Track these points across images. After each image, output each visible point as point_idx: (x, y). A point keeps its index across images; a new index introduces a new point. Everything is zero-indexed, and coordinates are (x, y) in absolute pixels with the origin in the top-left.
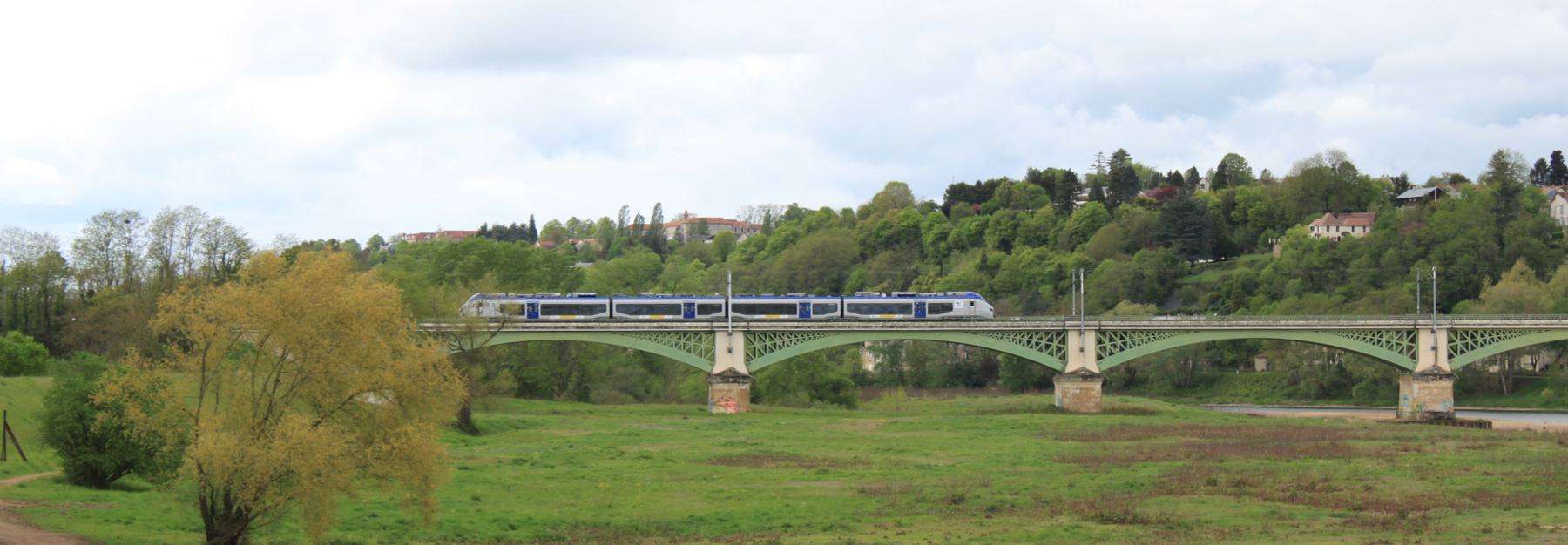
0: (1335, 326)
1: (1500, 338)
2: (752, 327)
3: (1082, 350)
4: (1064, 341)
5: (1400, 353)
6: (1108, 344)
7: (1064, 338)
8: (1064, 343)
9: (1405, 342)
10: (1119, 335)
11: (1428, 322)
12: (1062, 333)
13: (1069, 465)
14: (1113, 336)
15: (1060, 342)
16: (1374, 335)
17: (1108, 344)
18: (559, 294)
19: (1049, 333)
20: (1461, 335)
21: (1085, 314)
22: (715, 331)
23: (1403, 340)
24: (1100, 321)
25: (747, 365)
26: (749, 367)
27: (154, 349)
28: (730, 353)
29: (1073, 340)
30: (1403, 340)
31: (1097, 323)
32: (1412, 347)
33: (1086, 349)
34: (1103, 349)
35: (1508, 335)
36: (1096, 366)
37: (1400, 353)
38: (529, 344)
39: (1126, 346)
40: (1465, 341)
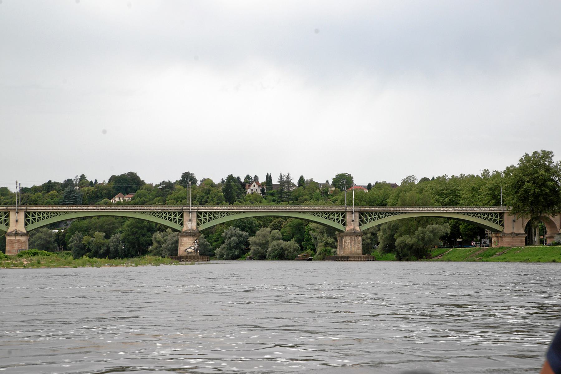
0: (203, 209)
1: (225, 215)
2: (362, 210)
3: (17, 221)
4: (8, 216)
5: (333, 221)
6: (202, 218)
7: (182, 215)
8: (345, 218)
9: (178, 217)
10: (208, 214)
11: (13, 208)
12: (7, 212)
13: (25, 270)
14: (39, 214)
15: (491, 217)
16: (326, 214)
17: (202, 218)
18: (159, 188)
19: (496, 214)
20: (370, 214)
21: (355, 205)
22: (9, 211)
23: (339, 217)
24: (27, 207)
25: (25, 228)
26: (27, 229)
27: (390, 225)
28: (190, 224)
29: (13, 217)
30: (339, 217)
31: (25, 208)
32: (344, 220)
33: (19, 220)
34: (362, 221)
35: (64, 213)
36: (25, 229)
37: (333, 221)
38: (145, 222)
39: (211, 219)
40: (39, 217)
